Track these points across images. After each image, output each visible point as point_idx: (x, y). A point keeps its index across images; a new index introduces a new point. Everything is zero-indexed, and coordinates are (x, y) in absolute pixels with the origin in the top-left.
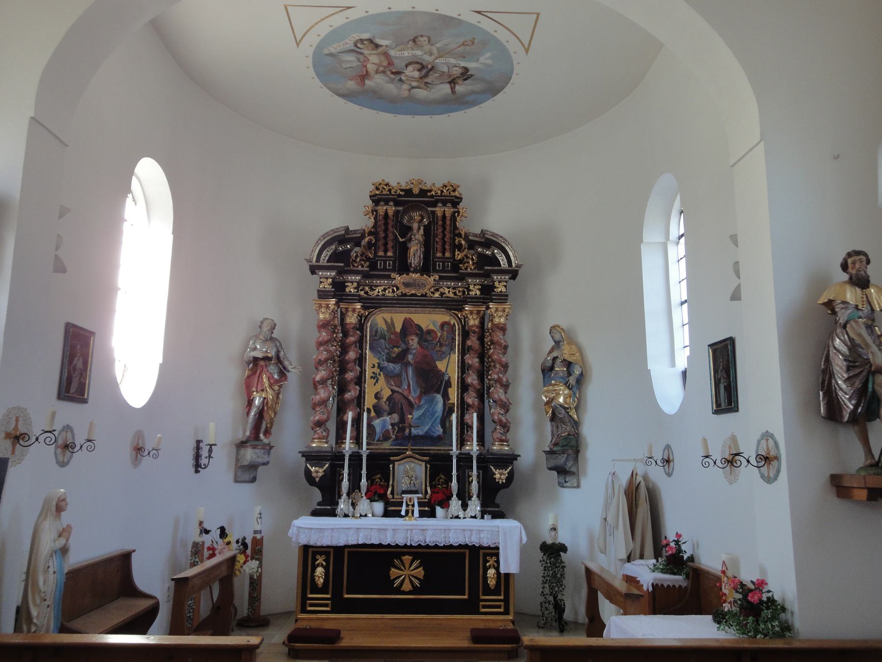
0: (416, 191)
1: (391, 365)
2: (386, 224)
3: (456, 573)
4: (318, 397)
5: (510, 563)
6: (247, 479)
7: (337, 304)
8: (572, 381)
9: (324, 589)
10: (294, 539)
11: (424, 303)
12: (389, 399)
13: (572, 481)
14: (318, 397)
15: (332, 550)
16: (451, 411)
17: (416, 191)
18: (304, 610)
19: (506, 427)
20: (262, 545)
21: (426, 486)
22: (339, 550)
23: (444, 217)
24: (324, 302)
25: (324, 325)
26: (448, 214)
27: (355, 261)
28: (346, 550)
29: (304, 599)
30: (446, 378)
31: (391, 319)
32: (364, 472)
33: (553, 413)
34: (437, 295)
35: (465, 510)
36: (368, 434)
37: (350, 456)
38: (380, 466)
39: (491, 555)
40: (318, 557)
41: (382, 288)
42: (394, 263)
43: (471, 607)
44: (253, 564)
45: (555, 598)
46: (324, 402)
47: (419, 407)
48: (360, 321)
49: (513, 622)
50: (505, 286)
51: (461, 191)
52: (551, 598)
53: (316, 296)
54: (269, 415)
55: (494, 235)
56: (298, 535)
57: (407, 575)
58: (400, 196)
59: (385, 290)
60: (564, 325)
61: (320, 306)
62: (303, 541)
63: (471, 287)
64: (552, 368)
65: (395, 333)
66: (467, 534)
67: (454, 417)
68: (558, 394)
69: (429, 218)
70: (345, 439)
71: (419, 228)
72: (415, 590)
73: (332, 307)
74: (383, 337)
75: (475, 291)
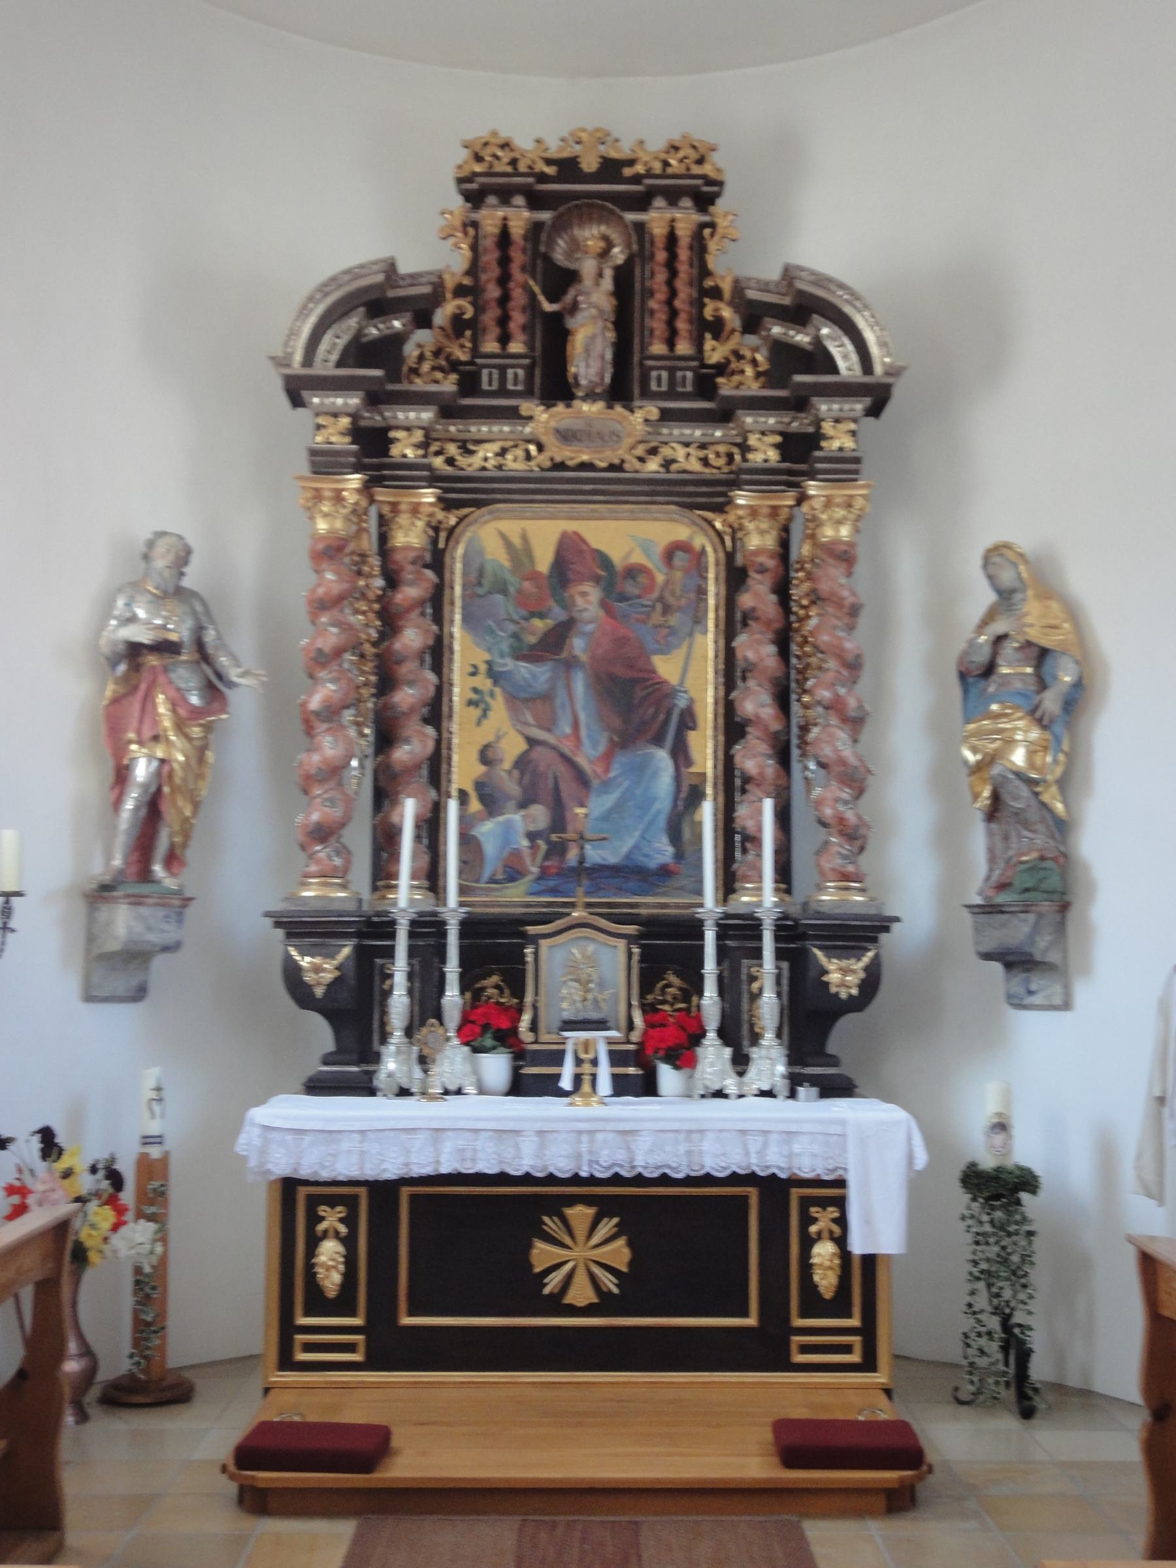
0: (590, 164)
1: (524, 669)
2: (504, 261)
3: (719, 1263)
4: (316, 758)
5: (878, 1223)
6: (121, 992)
7: (367, 488)
8: (1051, 702)
9: (344, 1303)
10: (253, 1163)
11: (611, 486)
12: (522, 763)
13: (1045, 987)
14: (316, 758)
15: (362, 1191)
16: (695, 796)
17: (590, 164)
18: (286, 1362)
19: (855, 836)
20: (165, 1176)
21: (630, 1006)
22: (383, 1193)
23: (672, 239)
24: (327, 485)
25: (330, 551)
26: (684, 232)
27: (415, 371)
28: (405, 1191)
29: (287, 1329)
30: (682, 703)
31: (524, 538)
32: (452, 968)
33: (996, 797)
34: (653, 465)
35: (741, 1074)
36: (463, 863)
37: (413, 923)
38: (497, 951)
39: (824, 1203)
40: (323, 1210)
41: (496, 447)
42: (530, 370)
43: (767, 1350)
44: (140, 1232)
45: (1006, 1326)
46: (334, 772)
47: (607, 785)
48: (435, 541)
49: (888, 1392)
50: (853, 433)
51: (721, 163)
52: (994, 1323)
53: (304, 468)
54: (175, 810)
55: (822, 280)
56: (263, 1152)
57: (582, 1259)
58: (542, 178)
59: (503, 452)
60: (1024, 541)
61: (318, 496)
62: (281, 1165)
63: (753, 440)
64: (989, 670)
65: (534, 576)
66: (754, 1144)
67: (707, 813)
68: (1010, 743)
69: (628, 245)
70: (395, 876)
71: (600, 275)
72: (605, 1304)
73: (351, 498)
74: (502, 588)
75: (765, 453)
